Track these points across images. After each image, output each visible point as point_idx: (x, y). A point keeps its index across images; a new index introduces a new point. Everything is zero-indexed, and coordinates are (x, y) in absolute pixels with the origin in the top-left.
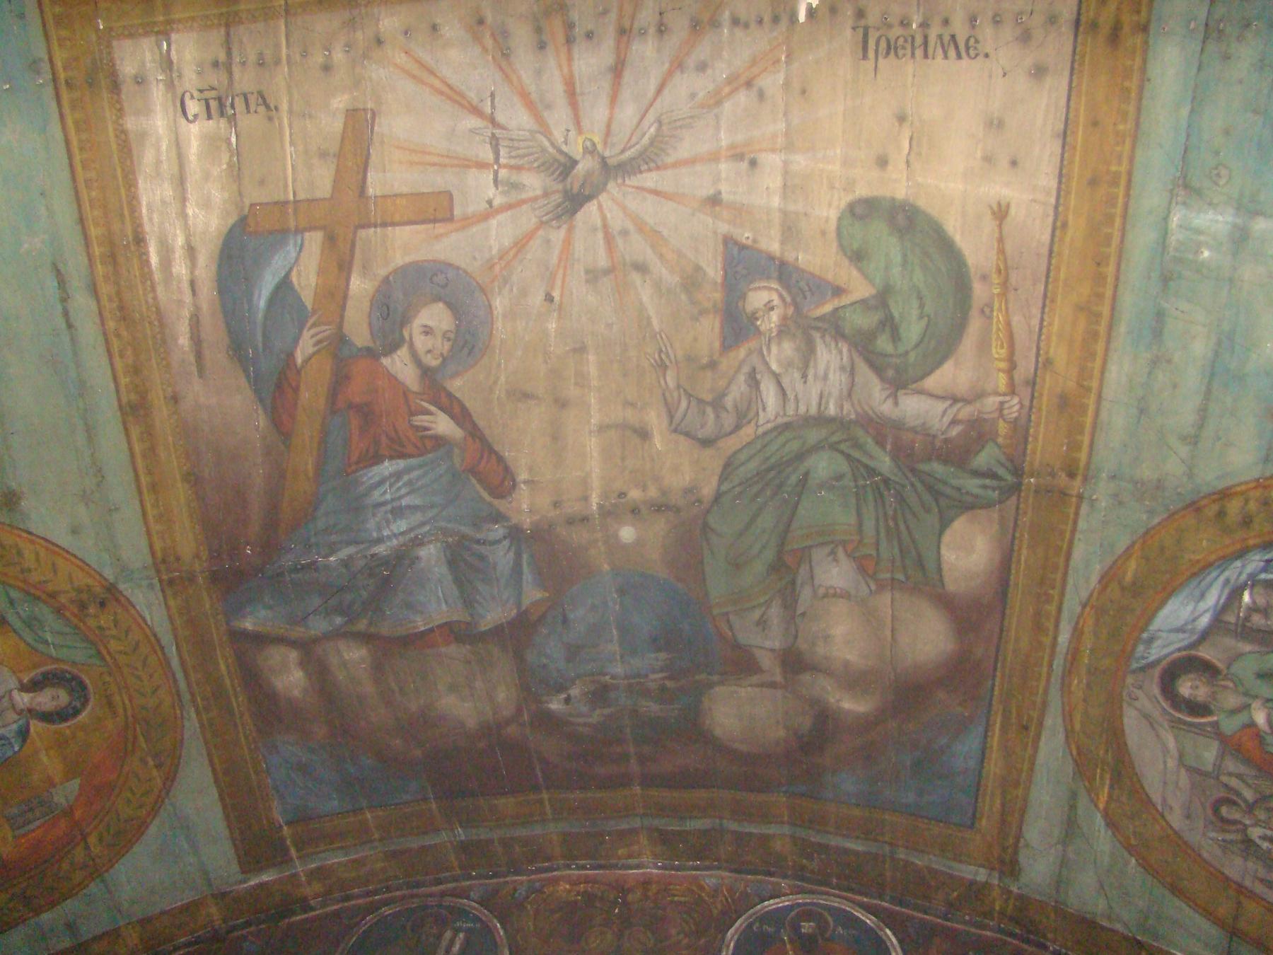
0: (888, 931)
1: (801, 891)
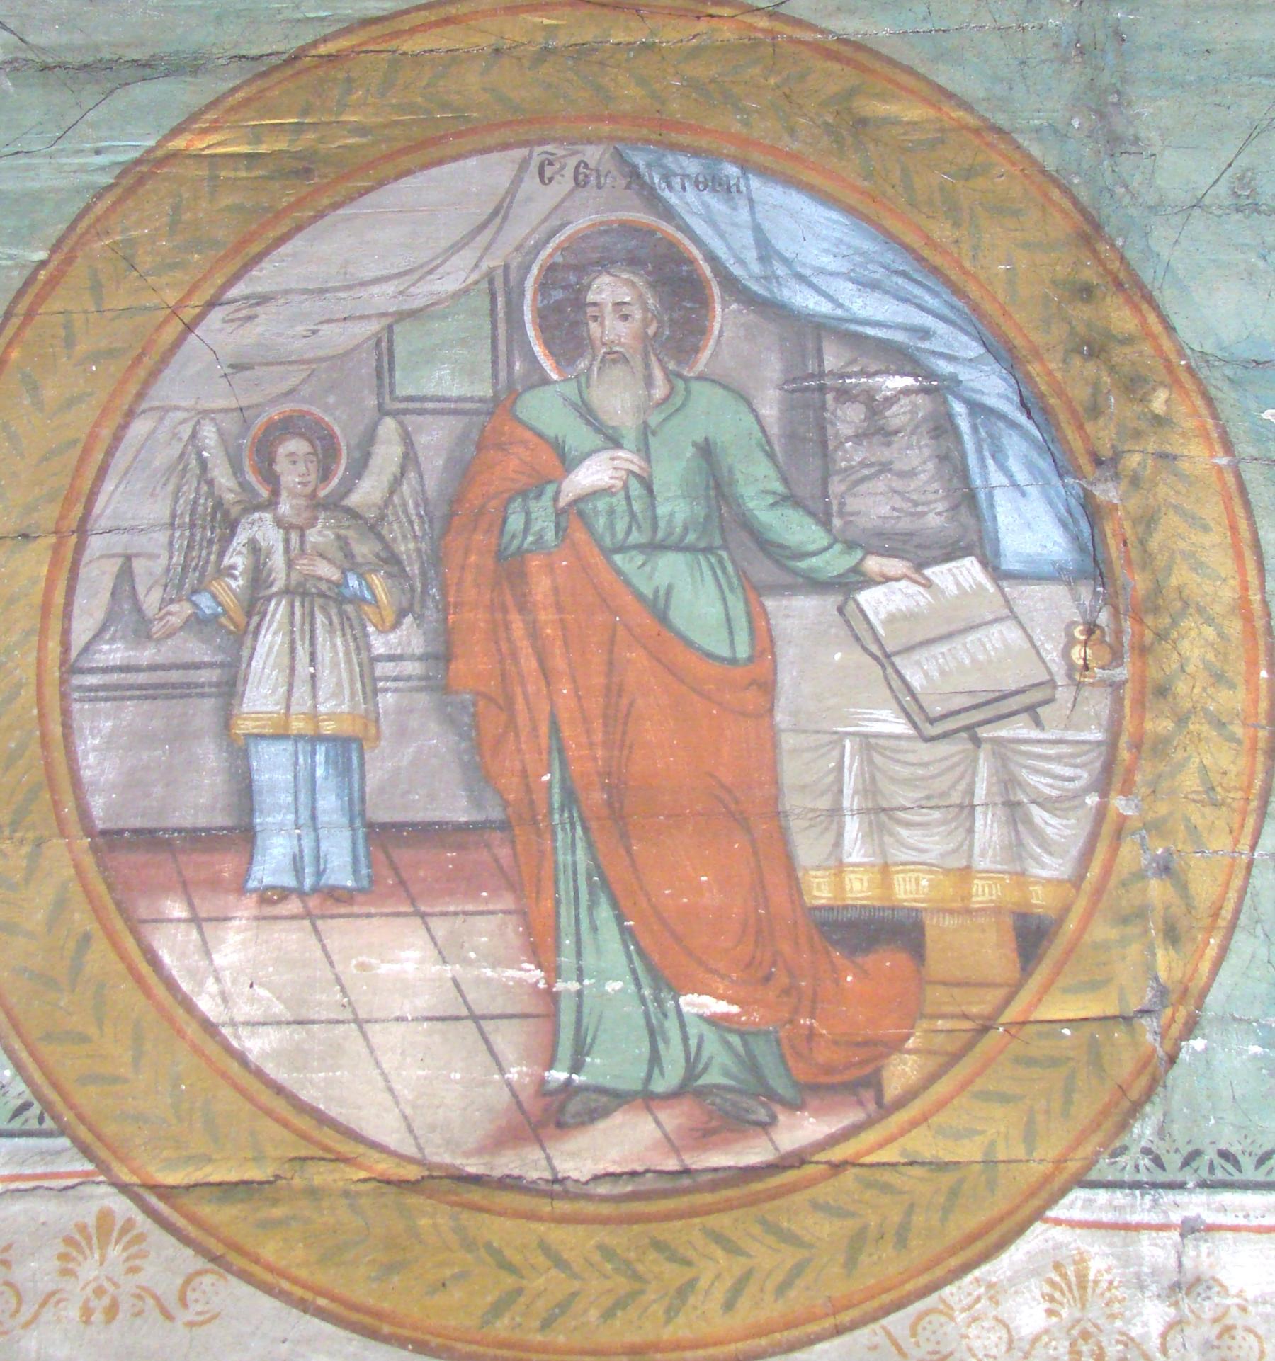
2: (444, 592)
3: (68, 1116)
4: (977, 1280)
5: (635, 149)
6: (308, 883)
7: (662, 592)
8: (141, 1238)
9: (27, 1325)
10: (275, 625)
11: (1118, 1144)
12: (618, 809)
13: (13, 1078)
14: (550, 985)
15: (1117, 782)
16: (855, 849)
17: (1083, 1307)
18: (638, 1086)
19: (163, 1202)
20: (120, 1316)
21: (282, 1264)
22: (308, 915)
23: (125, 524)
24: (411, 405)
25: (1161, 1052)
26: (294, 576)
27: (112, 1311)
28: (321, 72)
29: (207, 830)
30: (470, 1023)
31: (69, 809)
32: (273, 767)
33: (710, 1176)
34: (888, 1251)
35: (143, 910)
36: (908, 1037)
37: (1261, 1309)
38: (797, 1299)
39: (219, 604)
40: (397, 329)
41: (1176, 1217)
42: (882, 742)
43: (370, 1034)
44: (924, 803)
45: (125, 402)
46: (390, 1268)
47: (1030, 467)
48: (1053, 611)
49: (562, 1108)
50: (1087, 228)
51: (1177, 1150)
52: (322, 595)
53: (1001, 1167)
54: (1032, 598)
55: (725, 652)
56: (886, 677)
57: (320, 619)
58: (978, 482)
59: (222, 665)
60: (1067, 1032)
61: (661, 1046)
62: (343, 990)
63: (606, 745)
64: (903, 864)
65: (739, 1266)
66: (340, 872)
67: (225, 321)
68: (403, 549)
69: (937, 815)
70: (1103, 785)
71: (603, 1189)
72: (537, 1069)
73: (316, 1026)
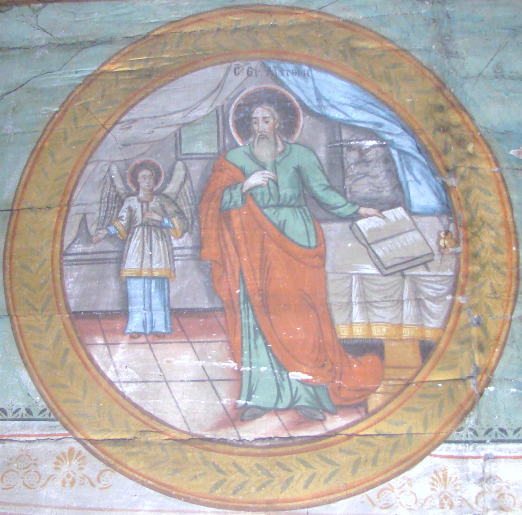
2: (200, 223)
3: (59, 414)
4: (404, 477)
5: (268, 61)
6: (148, 331)
7: (282, 222)
8: (84, 458)
9: (42, 486)
10: (137, 237)
11: (460, 426)
12: (266, 304)
13: (40, 400)
14: (239, 368)
15: (459, 291)
16: (357, 316)
17: (445, 487)
18: (272, 406)
19: (93, 446)
20: (75, 485)
21: (135, 468)
22: (148, 342)
23: (84, 202)
24: (188, 157)
25: (476, 392)
26: (144, 220)
28: (155, 41)
29: (112, 312)
30: (208, 384)
31: (62, 304)
32: (136, 288)
33: (300, 439)
34: (369, 467)
36: (377, 388)
37: (515, 487)
38: (333, 484)
39: (117, 230)
40: (183, 129)
41: (482, 454)
42: (367, 277)
43: (170, 386)
44: (384, 299)
45: (85, 159)
46: (176, 471)
47: (422, 173)
48: (433, 226)
49: (243, 414)
50: (440, 85)
51: (483, 428)
52: (155, 226)
53: (414, 436)
54: (424, 222)
55: (306, 244)
56: (368, 253)
57: (154, 234)
58: (402, 179)
59: (117, 252)
60: (440, 385)
61: (282, 391)
62: (161, 370)
63: (261, 279)
64: (376, 322)
65: (310, 472)
66: (160, 326)
67: (120, 129)
68: (185, 208)
69: (389, 304)
70: (453, 292)
71: (258, 444)
72: (234, 400)
73: (151, 383)
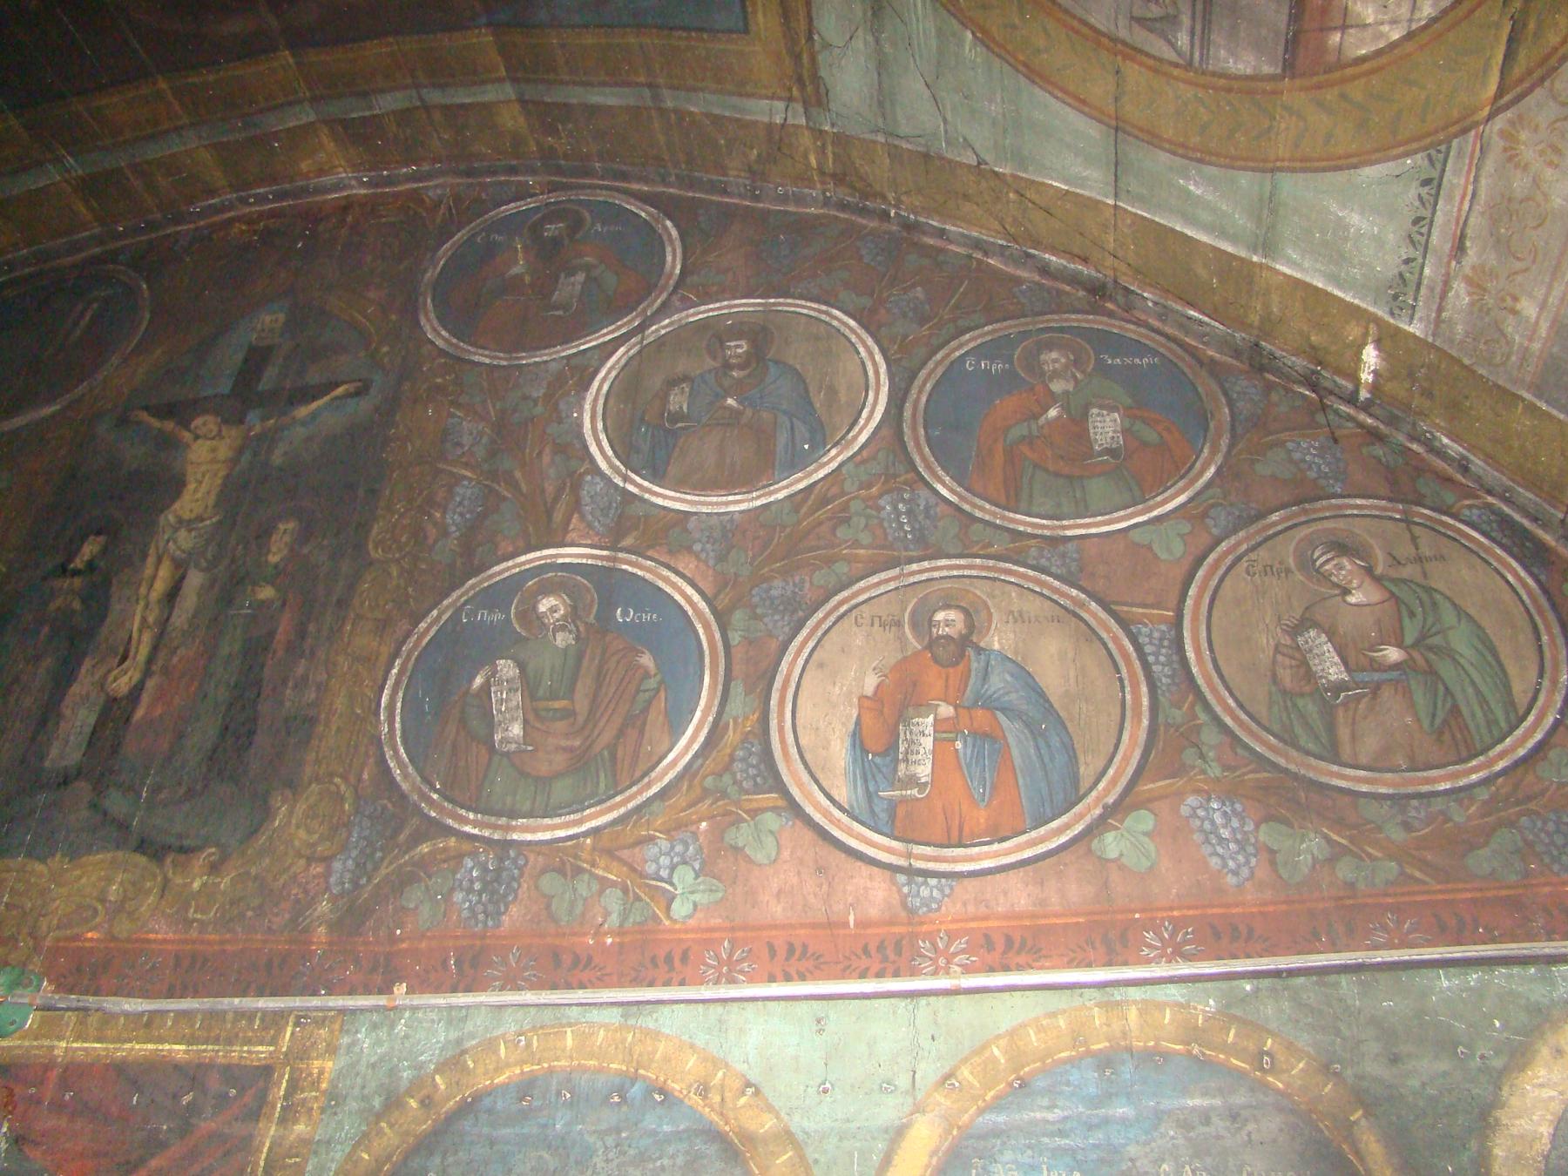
0: (669, 223)
1: (553, 188)
27: (1557, 150)
35: (1332, 58)
